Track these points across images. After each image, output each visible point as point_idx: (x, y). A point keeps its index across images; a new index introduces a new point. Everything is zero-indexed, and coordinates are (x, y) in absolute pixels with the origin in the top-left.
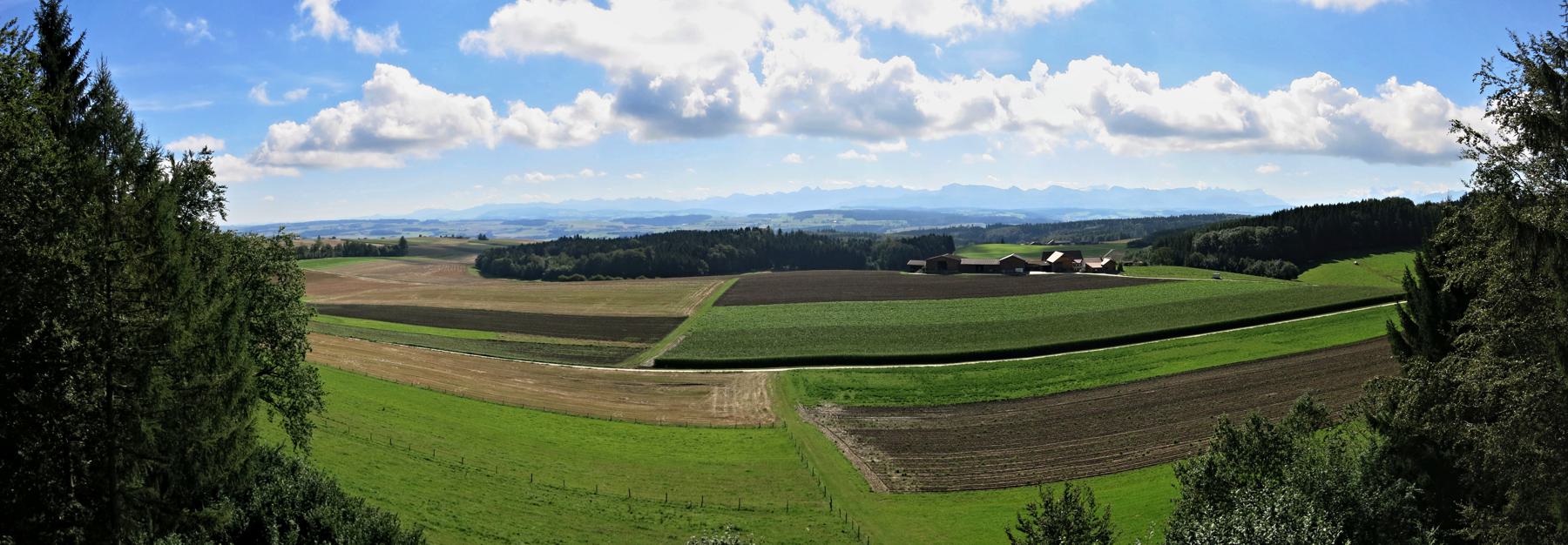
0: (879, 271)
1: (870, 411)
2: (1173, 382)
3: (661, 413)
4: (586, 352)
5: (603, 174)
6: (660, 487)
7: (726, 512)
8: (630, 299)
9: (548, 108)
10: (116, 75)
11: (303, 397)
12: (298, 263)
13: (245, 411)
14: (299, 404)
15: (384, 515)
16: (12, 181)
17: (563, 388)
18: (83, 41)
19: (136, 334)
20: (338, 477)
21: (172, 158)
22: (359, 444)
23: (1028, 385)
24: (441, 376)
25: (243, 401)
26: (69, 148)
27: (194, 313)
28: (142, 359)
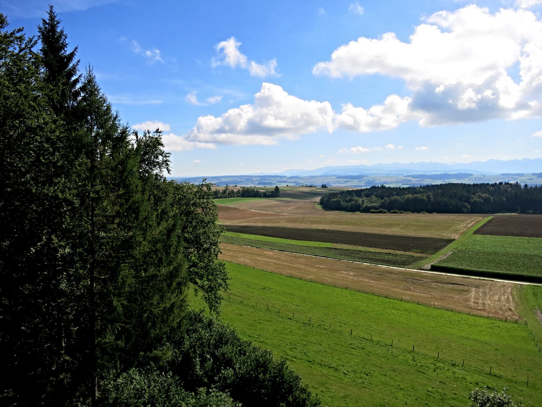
3: (434, 300)
4: (386, 257)
6: (434, 347)
8: (416, 225)
9: (367, 107)
10: (99, 79)
11: (216, 281)
12: (214, 200)
13: (181, 290)
14: (213, 285)
15: (263, 351)
16: (21, 141)
17: (372, 278)
18: (76, 53)
19: (111, 244)
20: (236, 329)
21: (136, 134)
22: (249, 309)
24: (298, 269)
25: (179, 284)
26: (65, 123)
27: (149, 230)
28: (115, 260)
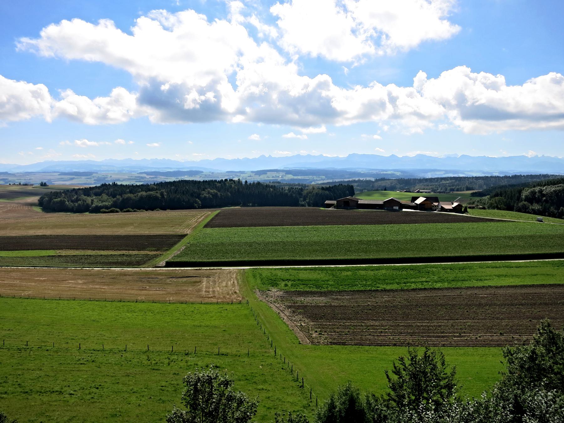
0: (307, 207)
1: (301, 294)
2: (501, 291)
3: (170, 295)
4: (120, 259)
5: (131, 142)
6: (168, 342)
7: (211, 356)
9: (92, 98)
17: (104, 284)
23: (398, 281)
